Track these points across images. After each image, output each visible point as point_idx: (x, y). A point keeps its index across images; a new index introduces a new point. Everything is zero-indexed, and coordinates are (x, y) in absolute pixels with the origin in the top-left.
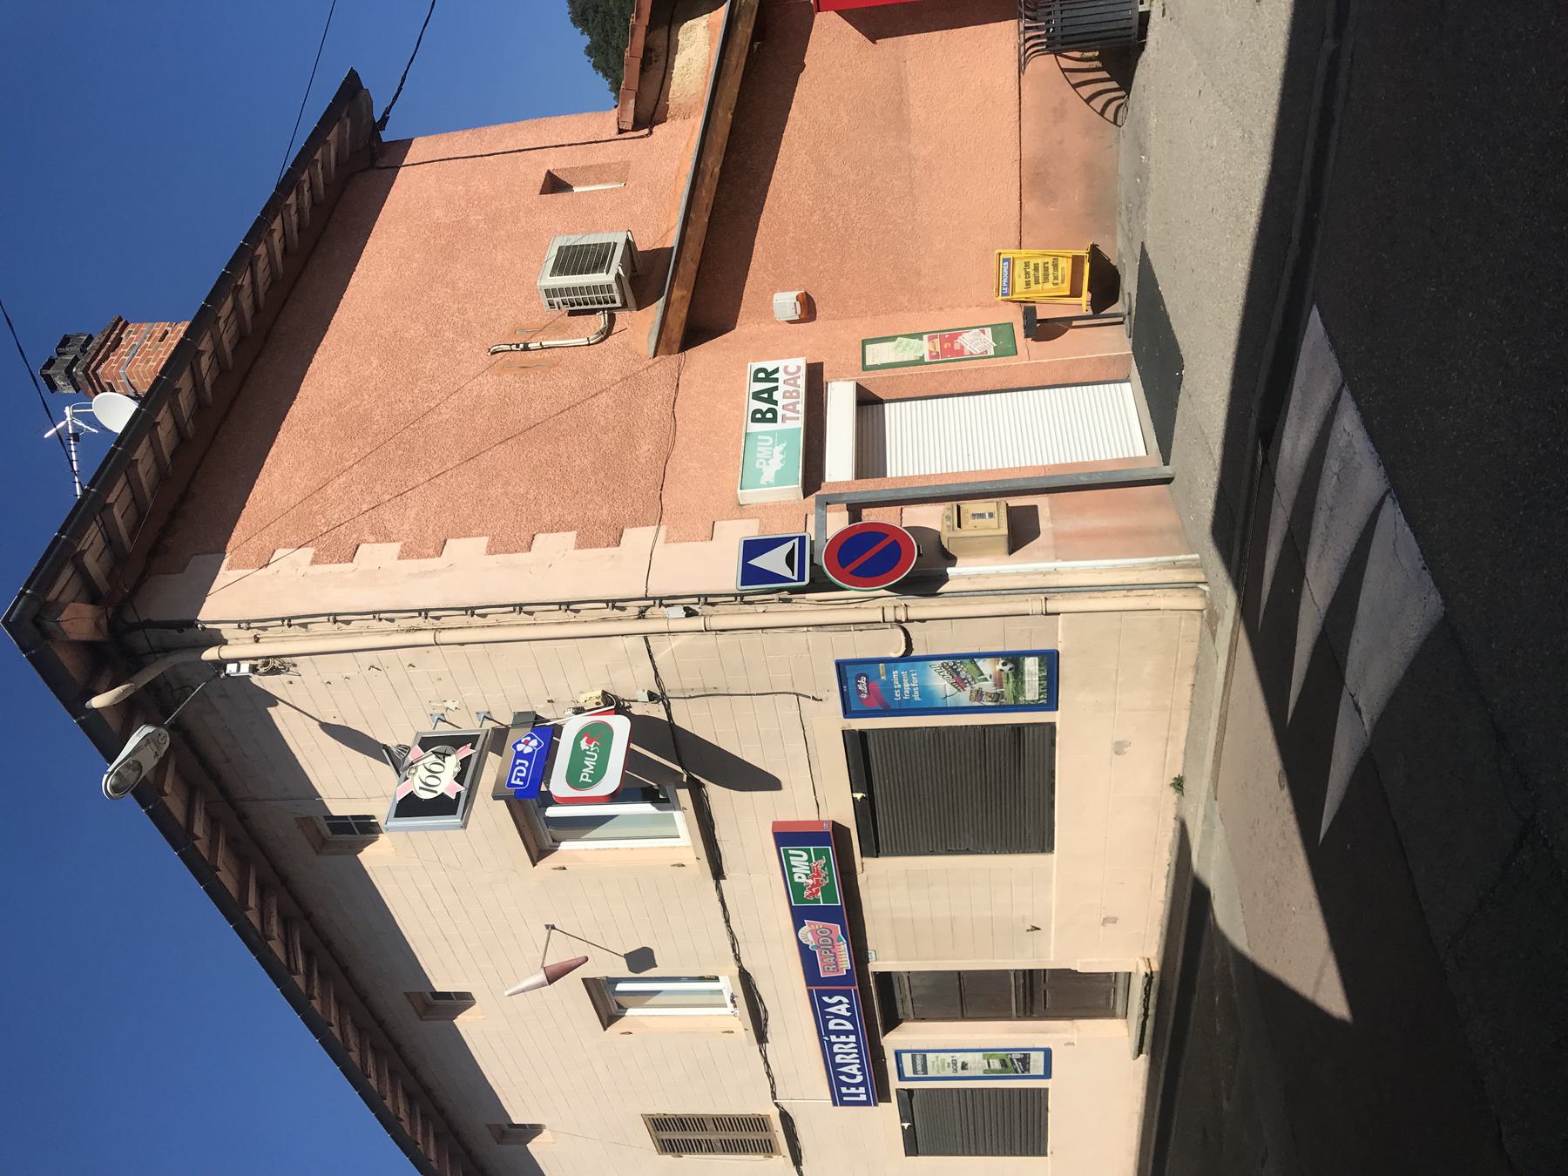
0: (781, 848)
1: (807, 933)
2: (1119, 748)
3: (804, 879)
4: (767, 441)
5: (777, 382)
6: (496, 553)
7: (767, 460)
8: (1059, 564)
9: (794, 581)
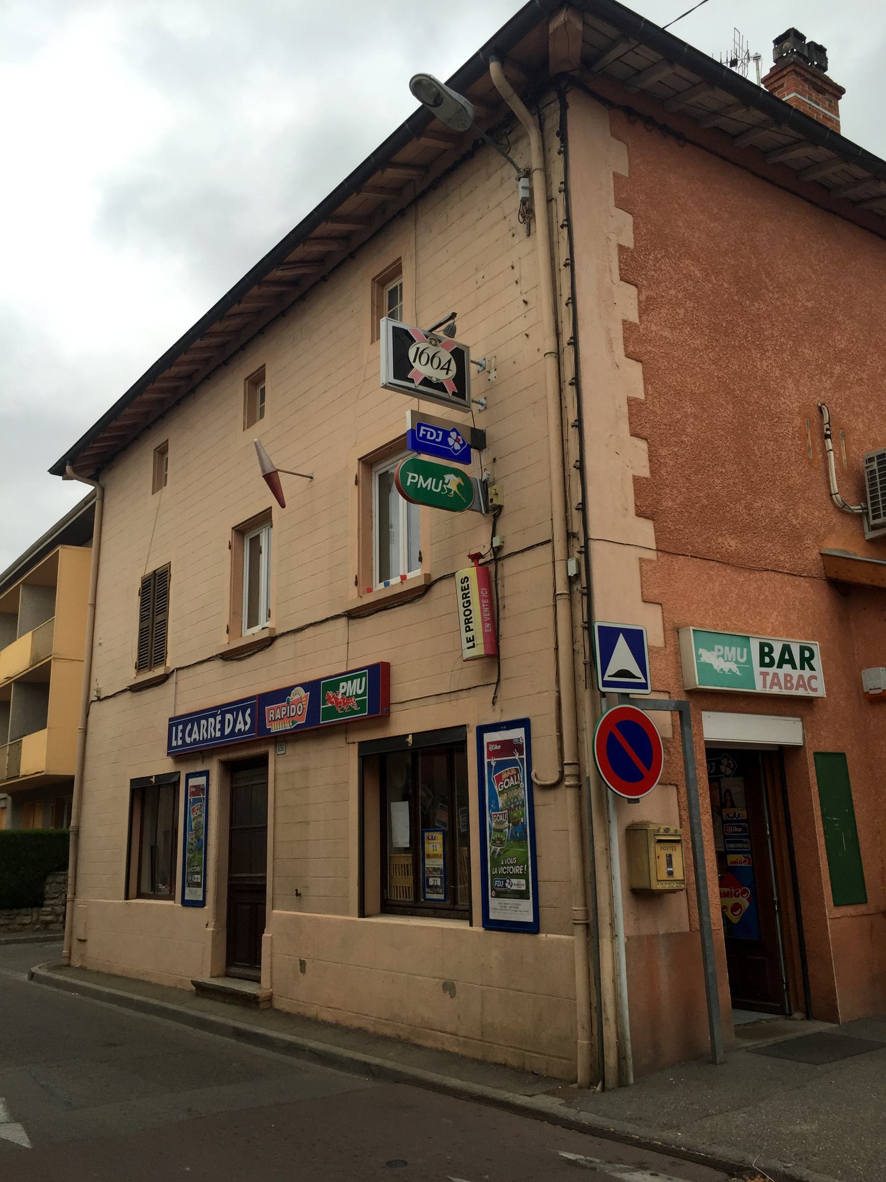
0: (367, 671)
1: (300, 694)
2: (449, 987)
3: (342, 691)
4: (742, 657)
5: (801, 669)
6: (629, 405)
7: (723, 656)
8: (622, 939)
9: (603, 676)
